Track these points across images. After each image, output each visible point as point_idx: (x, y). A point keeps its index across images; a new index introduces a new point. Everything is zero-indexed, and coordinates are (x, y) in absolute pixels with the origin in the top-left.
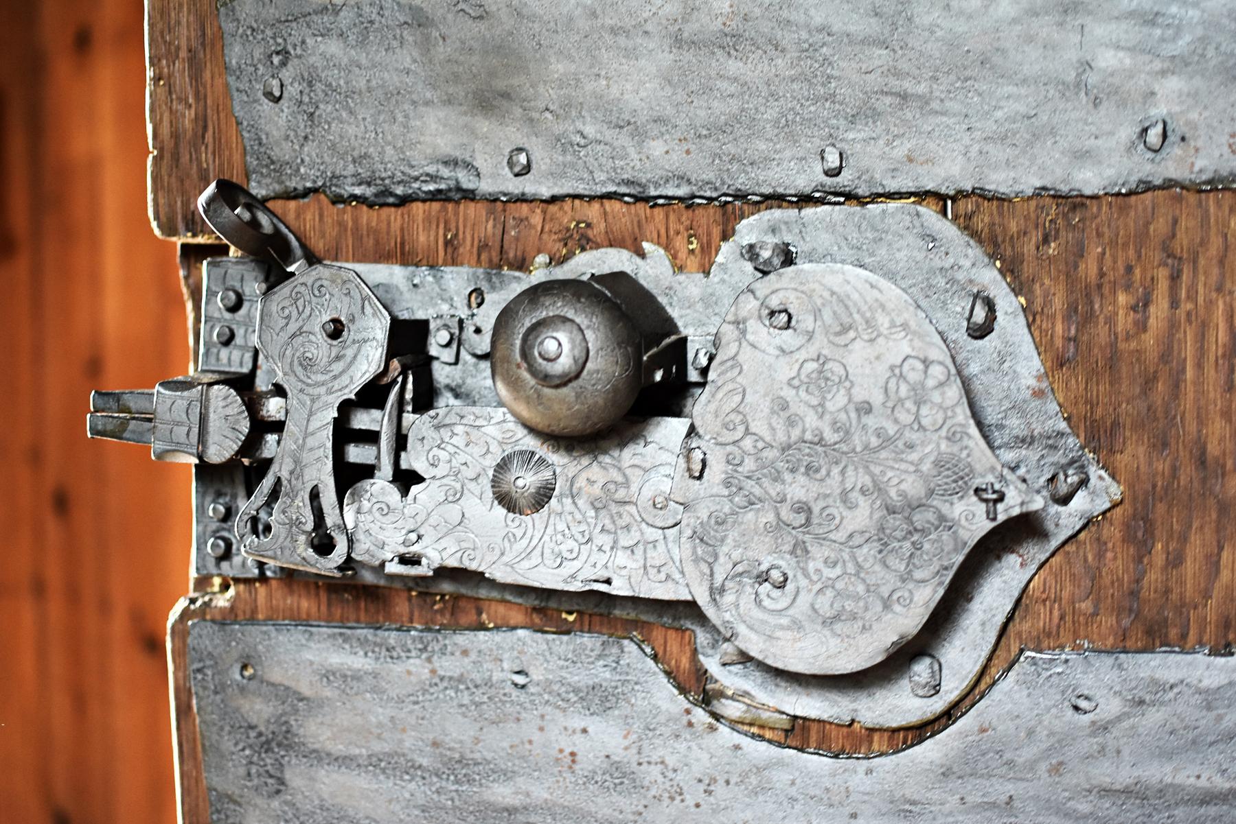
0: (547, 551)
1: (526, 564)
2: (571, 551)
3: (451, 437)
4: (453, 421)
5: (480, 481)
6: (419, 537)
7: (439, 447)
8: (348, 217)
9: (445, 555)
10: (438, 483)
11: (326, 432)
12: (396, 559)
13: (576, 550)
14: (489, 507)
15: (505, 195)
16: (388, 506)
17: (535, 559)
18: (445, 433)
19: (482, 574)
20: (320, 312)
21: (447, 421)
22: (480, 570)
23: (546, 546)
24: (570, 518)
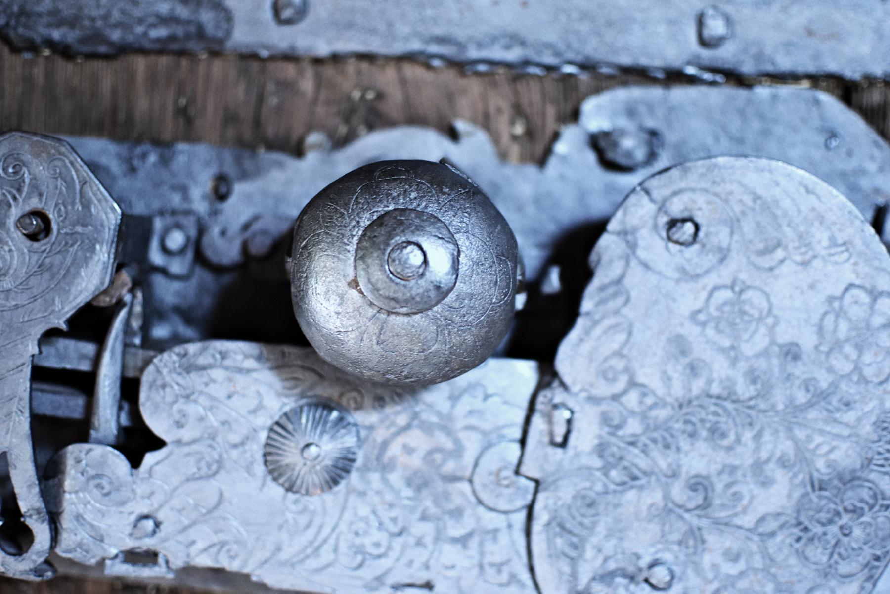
0: (343, 547)
1: (312, 563)
2: (377, 545)
3: (206, 385)
4: (210, 360)
5: (247, 447)
6: (157, 525)
7: (187, 397)
8: (39, 72)
9: (193, 550)
10: (186, 449)
11: (23, 374)
12: (121, 556)
13: (384, 543)
14: (259, 484)
15: (266, 47)
16: (111, 483)
17: (326, 555)
18: (195, 380)
19: (247, 577)
20: (15, 198)
21: (201, 361)
22: (245, 571)
23: (342, 538)
24: (376, 499)
